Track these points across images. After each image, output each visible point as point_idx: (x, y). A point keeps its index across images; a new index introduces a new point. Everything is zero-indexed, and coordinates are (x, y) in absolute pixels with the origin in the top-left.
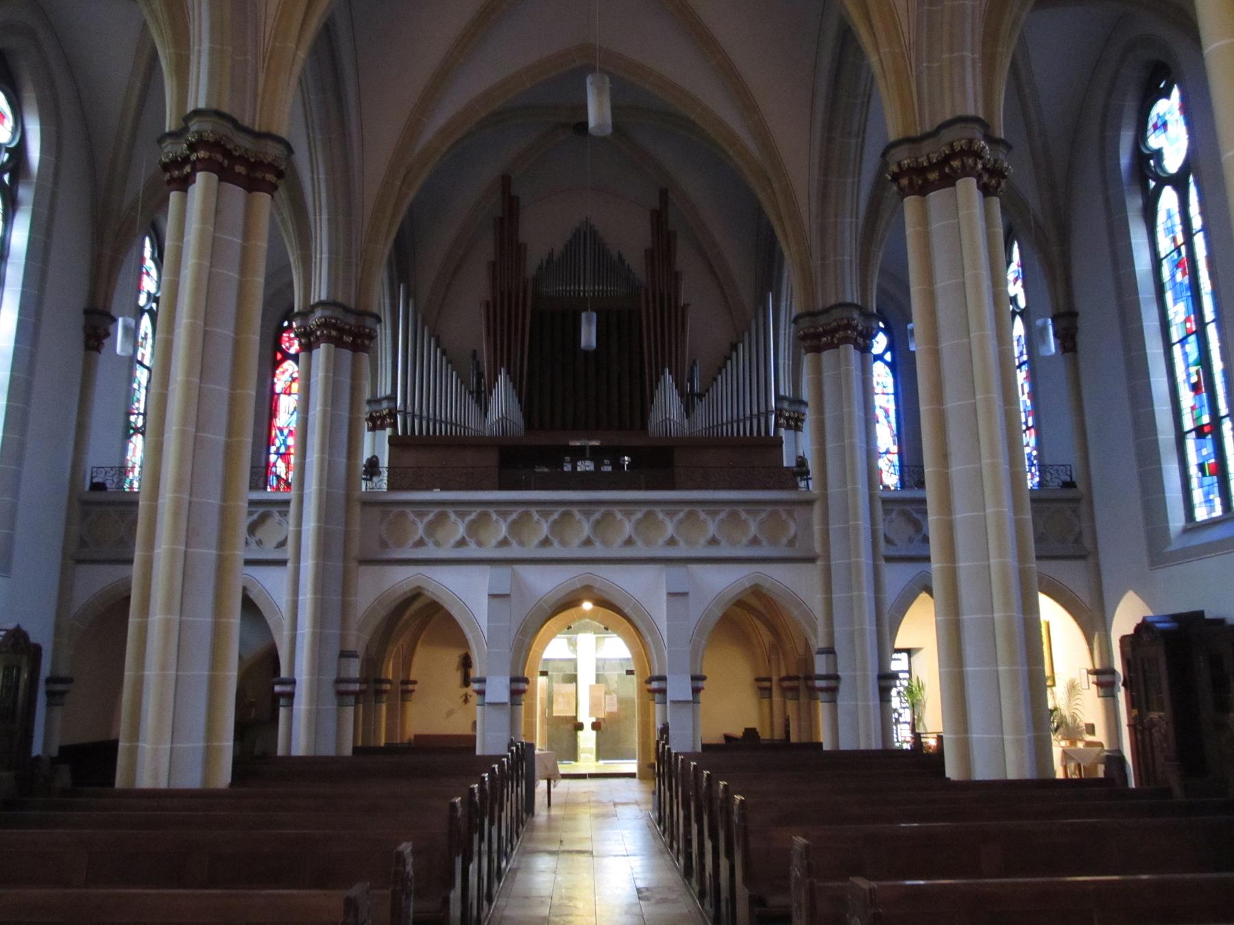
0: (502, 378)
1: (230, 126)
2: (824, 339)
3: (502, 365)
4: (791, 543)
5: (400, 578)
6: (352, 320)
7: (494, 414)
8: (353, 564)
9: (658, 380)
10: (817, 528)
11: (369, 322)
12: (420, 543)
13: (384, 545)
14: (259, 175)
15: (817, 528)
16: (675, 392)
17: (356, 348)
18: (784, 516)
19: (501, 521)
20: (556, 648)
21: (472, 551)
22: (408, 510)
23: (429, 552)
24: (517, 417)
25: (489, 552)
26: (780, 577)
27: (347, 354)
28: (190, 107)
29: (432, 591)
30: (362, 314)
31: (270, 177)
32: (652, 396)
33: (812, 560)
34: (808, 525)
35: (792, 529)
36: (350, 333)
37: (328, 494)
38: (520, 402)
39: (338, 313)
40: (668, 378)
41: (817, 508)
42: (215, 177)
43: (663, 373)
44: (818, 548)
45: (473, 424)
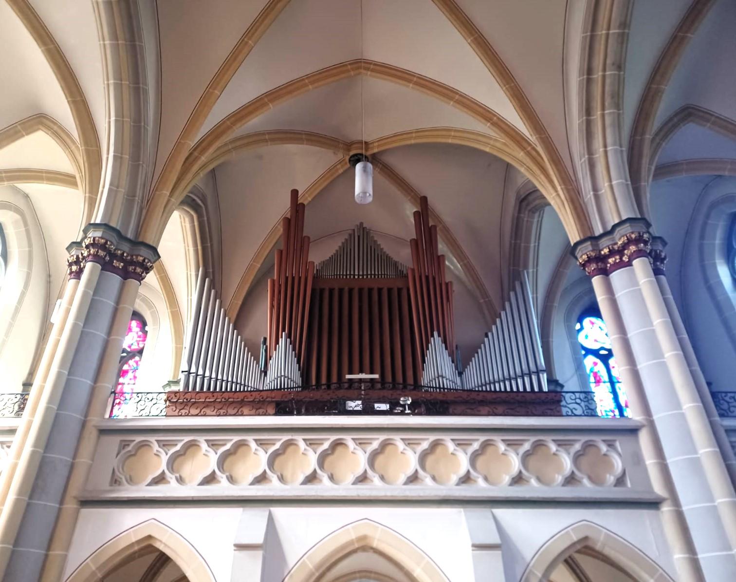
0: (282, 341)
1: (115, 235)
2: (611, 260)
3: (284, 330)
4: (620, 481)
5: (127, 526)
6: (126, 247)
7: (272, 374)
8: (70, 505)
9: (428, 342)
10: (650, 461)
11: (144, 252)
12: (160, 479)
13: (115, 481)
14: (131, 268)
15: (650, 461)
16: (446, 353)
17: (126, 275)
18: (604, 448)
19: (261, 452)
20: (628, 260)
21: (222, 488)
22: (153, 439)
23: (171, 489)
24: (296, 378)
25: (244, 490)
26: (614, 527)
27: (115, 280)
28: (92, 222)
29: (167, 544)
30: (137, 243)
31: (139, 270)
32: (423, 356)
33: (654, 504)
34: (637, 459)
35: (618, 464)
36: (121, 258)
37: (57, 416)
38: (299, 362)
39: (114, 238)
40: (436, 341)
41: (644, 437)
42: (99, 267)
43: (432, 336)
44: (658, 489)
45: (254, 382)
